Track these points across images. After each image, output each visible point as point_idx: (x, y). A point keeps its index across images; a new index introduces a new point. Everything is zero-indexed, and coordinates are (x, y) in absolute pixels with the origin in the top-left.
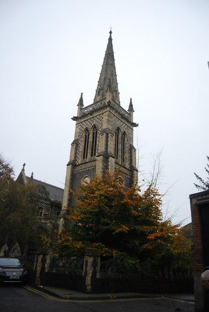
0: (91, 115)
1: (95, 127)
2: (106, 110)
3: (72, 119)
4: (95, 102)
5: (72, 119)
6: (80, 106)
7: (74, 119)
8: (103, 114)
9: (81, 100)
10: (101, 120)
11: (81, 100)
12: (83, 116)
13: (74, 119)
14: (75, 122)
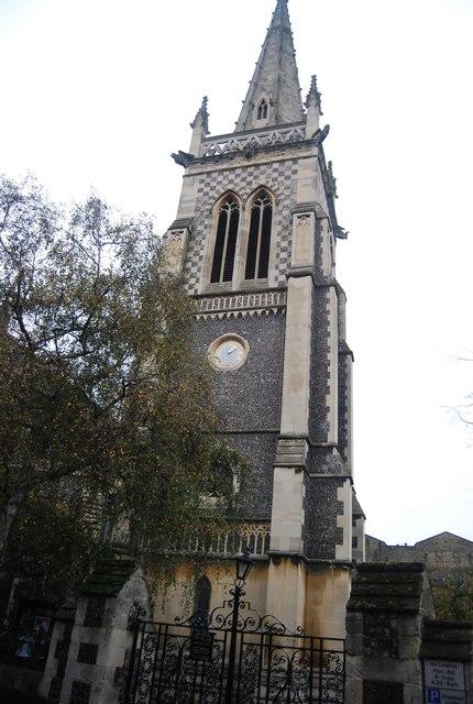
0: (248, 157)
1: (262, 193)
2: (200, 170)
3: (173, 156)
4: (243, 129)
5: (173, 156)
6: (200, 129)
7: (183, 159)
8: (295, 160)
9: (203, 115)
10: (288, 178)
11: (203, 115)
12: (177, 162)
13: (183, 159)
14: (181, 170)
